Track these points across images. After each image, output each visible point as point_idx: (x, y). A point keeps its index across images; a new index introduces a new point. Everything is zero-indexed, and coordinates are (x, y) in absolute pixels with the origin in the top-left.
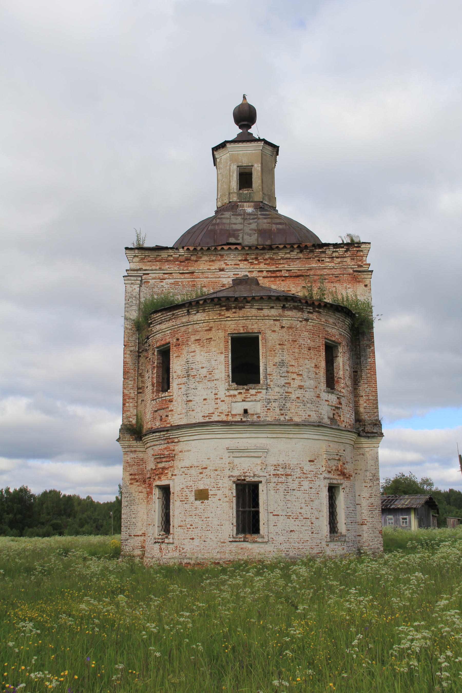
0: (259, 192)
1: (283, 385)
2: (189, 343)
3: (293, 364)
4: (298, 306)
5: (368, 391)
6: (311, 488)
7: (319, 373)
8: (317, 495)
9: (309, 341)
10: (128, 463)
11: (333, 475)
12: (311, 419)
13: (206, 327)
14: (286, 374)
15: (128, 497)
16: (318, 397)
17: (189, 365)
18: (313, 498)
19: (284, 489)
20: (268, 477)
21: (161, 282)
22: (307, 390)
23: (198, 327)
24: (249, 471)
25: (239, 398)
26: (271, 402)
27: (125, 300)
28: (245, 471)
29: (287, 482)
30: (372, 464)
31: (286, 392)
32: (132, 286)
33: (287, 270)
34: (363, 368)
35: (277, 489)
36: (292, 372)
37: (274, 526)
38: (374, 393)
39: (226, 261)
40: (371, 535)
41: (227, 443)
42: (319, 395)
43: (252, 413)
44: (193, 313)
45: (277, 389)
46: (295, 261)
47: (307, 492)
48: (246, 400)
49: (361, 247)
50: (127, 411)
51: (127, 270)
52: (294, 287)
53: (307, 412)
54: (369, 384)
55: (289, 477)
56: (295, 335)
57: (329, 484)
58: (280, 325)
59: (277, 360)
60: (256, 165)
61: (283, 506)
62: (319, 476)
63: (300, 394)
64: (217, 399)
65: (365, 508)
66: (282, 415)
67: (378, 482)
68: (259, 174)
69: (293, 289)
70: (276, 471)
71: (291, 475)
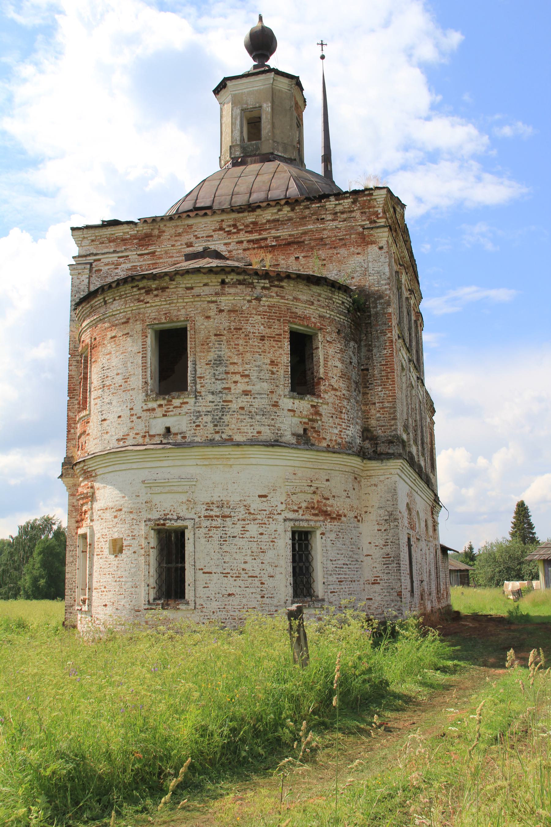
0: (268, 140)
1: (220, 392)
2: (105, 342)
3: (235, 361)
4: (244, 280)
5: (382, 395)
6: (261, 534)
7: (278, 371)
8: (272, 544)
9: (262, 327)
10: (73, 506)
11: (302, 515)
12: (262, 438)
13: (123, 318)
14: (225, 376)
15: (73, 551)
16: (273, 405)
17: (105, 371)
18: (265, 548)
19: (219, 536)
20: (197, 520)
21: (116, 268)
22: (256, 396)
23: (115, 319)
24: (172, 512)
25: (159, 412)
26: (201, 416)
27: (72, 296)
28: (166, 512)
29: (224, 527)
30: (389, 498)
31: (224, 401)
32: (80, 276)
33: (274, 237)
34: (375, 364)
35: (210, 537)
36: (233, 373)
37: (204, 587)
38: (390, 398)
39: (196, 233)
40: (386, 598)
41: (144, 474)
42: (277, 402)
43: (176, 432)
44: (109, 301)
45: (210, 397)
46: (285, 224)
47: (255, 540)
48: (168, 414)
49: (374, 194)
50: (72, 439)
51: (74, 257)
52: (284, 259)
53: (255, 427)
54: (384, 385)
55: (228, 519)
56: (240, 320)
57: (292, 527)
58: (217, 308)
59: (211, 356)
60: (265, 105)
61: (218, 559)
62: (275, 517)
63: (245, 403)
64: (132, 415)
65: (378, 560)
66: (217, 432)
67: (396, 523)
68: (269, 117)
69: (283, 262)
70: (208, 512)
71: (231, 517)
